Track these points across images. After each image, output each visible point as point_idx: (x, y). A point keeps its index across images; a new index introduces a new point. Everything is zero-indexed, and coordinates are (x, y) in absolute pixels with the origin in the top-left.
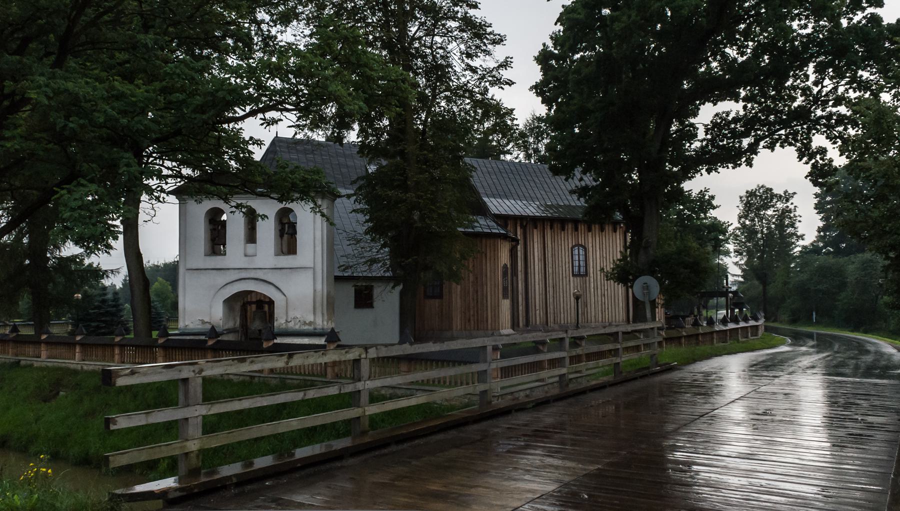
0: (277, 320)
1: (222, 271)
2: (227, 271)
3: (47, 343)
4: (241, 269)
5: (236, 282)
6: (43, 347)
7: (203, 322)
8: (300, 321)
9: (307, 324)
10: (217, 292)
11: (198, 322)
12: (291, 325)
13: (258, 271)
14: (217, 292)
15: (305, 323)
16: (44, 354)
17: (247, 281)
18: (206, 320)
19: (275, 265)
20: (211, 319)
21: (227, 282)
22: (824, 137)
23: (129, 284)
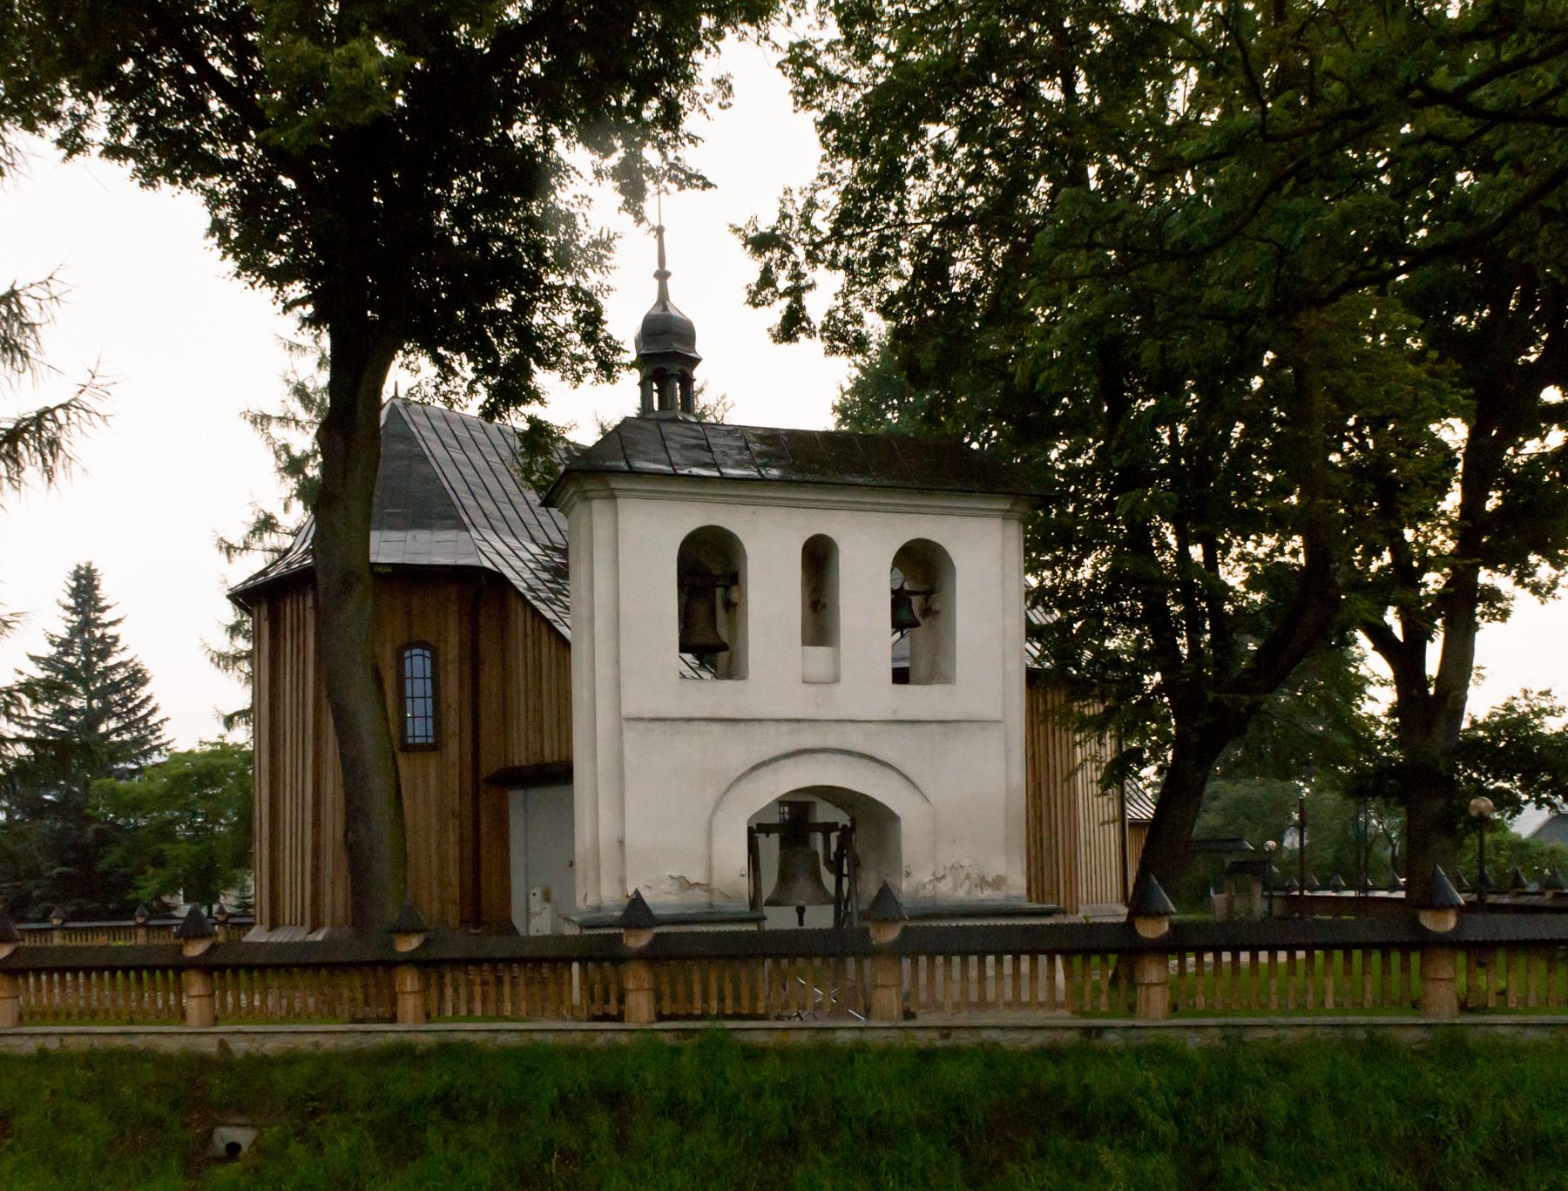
0: (908, 874)
1: (742, 725)
2: (757, 725)
3: (206, 967)
4: (798, 721)
5: (789, 763)
6: (196, 984)
7: (685, 884)
8: (968, 876)
9: (987, 883)
10: (729, 789)
11: (666, 886)
12: (945, 887)
13: (849, 727)
14: (729, 789)
15: (983, 882)
16: (409, 1005)
17: (821, 756)
18: (696, 876)
19: (895, 712)
20: (710, 876)
21: (757, 760)
22: (777, 300)
23: (103, 734)
